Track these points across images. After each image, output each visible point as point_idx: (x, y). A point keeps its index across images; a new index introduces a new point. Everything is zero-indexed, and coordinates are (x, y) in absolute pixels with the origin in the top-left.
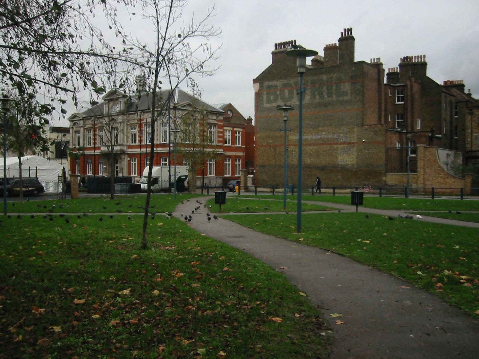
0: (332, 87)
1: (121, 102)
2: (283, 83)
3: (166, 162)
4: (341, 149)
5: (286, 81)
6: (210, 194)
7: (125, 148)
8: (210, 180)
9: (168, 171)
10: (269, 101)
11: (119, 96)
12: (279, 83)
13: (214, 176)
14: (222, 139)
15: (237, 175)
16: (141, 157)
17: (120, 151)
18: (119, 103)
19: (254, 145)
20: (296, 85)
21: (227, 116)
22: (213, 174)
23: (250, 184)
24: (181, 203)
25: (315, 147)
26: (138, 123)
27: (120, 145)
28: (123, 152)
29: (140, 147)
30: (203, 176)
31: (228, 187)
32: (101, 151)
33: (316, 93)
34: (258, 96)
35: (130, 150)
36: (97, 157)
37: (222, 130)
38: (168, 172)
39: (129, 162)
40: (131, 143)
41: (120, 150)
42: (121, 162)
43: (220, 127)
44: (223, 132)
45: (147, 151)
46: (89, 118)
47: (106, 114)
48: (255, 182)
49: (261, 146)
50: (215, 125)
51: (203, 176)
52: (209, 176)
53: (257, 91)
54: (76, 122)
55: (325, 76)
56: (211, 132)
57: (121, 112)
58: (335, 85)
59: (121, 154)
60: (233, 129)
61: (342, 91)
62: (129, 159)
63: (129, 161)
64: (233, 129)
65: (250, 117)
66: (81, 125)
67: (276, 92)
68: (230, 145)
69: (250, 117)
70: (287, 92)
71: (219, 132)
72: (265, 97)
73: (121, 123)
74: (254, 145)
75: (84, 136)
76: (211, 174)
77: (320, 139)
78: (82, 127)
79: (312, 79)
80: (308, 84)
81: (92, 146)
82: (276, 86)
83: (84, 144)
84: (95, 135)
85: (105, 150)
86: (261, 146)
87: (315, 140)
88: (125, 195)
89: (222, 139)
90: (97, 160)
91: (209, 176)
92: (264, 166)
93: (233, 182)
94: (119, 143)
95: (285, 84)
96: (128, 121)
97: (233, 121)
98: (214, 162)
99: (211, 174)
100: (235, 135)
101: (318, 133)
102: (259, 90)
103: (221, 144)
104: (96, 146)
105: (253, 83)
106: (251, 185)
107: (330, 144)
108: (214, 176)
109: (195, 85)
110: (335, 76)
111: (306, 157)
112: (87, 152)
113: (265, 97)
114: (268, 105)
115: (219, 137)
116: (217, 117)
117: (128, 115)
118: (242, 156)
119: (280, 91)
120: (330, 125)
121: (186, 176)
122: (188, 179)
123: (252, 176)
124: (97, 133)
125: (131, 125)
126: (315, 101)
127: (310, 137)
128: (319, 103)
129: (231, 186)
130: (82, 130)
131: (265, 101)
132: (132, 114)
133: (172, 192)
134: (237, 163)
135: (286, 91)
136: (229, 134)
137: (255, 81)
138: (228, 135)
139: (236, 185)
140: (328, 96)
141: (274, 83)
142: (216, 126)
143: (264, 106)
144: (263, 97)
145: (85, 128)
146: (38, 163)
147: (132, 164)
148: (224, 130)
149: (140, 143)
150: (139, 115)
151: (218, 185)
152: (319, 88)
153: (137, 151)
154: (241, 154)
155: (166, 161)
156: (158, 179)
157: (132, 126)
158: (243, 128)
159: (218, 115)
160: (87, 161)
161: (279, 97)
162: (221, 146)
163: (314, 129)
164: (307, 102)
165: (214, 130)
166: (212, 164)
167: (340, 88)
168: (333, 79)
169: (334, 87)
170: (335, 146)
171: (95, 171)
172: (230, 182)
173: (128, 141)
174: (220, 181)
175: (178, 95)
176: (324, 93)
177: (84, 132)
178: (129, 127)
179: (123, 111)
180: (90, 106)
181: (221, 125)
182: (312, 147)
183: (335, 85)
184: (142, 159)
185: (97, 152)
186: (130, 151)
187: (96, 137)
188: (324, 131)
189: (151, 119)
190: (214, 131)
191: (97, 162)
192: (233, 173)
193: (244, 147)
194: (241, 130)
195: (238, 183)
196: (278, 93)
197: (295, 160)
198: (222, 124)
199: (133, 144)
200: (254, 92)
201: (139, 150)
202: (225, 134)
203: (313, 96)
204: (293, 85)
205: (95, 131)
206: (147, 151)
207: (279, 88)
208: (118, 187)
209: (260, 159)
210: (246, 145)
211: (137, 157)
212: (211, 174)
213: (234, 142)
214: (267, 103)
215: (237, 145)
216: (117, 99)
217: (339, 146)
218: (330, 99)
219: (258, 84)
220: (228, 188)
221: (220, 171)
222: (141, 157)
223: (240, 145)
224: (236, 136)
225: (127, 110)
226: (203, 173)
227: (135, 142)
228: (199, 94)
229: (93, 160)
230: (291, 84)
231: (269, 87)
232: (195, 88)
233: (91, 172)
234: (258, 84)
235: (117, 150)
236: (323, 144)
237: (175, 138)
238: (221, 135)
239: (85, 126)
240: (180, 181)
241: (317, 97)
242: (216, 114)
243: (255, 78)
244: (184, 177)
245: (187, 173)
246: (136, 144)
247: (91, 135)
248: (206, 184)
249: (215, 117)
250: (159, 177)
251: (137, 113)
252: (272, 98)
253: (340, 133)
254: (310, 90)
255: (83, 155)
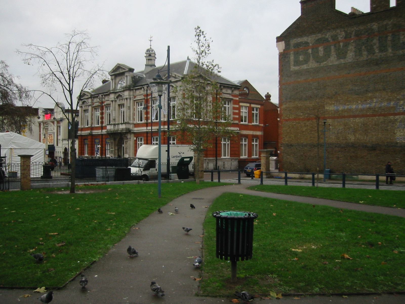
0: (387, 37)
1: (127, 76)
2: (317, 38)
3: (174, 142)
4: (401, 122)
5: (320, 36)
6: (222, 181)
7: (131, 127)
8: (224, 162)
9: (166, 151)
10: (297, 63)
11: (126, 70)
12: (310, 39)
13: (229, 157)
14: (237, 116)
15: (254, 157)
16: (147, 137)
17: (126, 130)
18: (126, 78)
19: (279, 119)
20: (333, 40)
21: (243, 92)
22: (228, 156)
23: (272, 168)
24: (157, 212)
25: (362, 120)
26: (144, 99)
27: (126, 123)
28: (129, 131)
29: (147, 125)
30: (216, 157)
31: (245, 171)
32: (107, 130)
33: (363, 47)
34: (283, 57)
35: (136, 129)
36: (104, 137)
37: (237, 106)
38: (167, 152)
39: (136, 141)
40: (137, 121)
41: (126, 128)
42: (126, 143)
43: (236, 102)
44: (239, 109)
45: (152, 129)
46: (97, 95)
47: (112, 91)
48: (280, 166)
49: (286, 120)
50: (230, 100)
51: (216, 157)
52: (223, 157)
53: (282, 51)
54: (85, 100)
55: (376, 24)
56: (225, 108)
57: (127, 87)
58: (390, 34)
59: (126, 133)
60: (250, 105)
61: (401, 42)
62: (135, 138)
63: (135, 140)
64: (250, 105)
65: (268, 93)
66: (89, 104)
67: (308, 50)
68: (247, 123)
69: (268, 93)
70: (322, 49)
71: (234, 108)
72: (292, 58)
73: (127, 99)
74: (279, 119)
75: (92, 115)
76: (225, 156)
77: (370, 108)
78: (90, 105)
79: (357, 29)
80: (351, 37)
81: (100, 125)
82: (307, 43)
83: (92, 124)
84: (102, 114)
85: (111, 129)
86: (286, 120)
87: (362, 110)
88: (103, 184)
89: (237, 116)
90: (104, 140)
91: (223, 157)
92: (291, 145)
93: (252, 165)
94: (125, 121)
95: (318, 39)
96: (135, 97)
97: (250, 97)
98: (228, 141)
99: (226, 156)
100: (253, 112)
101: (366, 101)
102: (284, 50)
103: (236, 122)
104: (104, 125)
105: (277, 41)
106: (274, 169)
107: (384, 115)
108: (229, 157)
109: (201, 34)
110: (390, 23)
111: (349, 134)
112: (95, 132)
113: (292, 58)
114: (297, 68)
115: (234, 114)
116: (233, 91)
117: (134, 90)
118: (260, 135)
119: (313, 49)
120: (384, 89)
121: (191, 158)
122: (193, 161)
123: (275, 158)
124: (104, 111)
125: (137, 101)
126: (361, 59)
127: (354, 107)
128: (367, 60)
129: (249, 170)
130: (90, 108)
131: (292, 63)
132: (138, 89)
133: (171, 179)
134: (254, 143)
135: (321, 49)
136: (246, 111)
137: (279, 39)
138: (244, 112)
139: (254, 168)
140: (381, 51)
141: (305, 39)
142: (230, 101)
143: (291, 70)
144: (290, 58)
145: (94, 107)
146: (13, 141)
147: (139, 144)
148: (240, 107)
149: (147, 121)
150: (146, 90)
151: (233, 168)
152: (367, 41)
153: (144, 129)
154: (259, 133)
155: (174, 140)
156: (155, 161)
157: (138, 102)
158: (261, 105)
159: (233, 89)
160: (95, 141)
161: (311, 57)
162: (237, 124)
163: (361, 96)
164: (350, 61)
165: (228, 106)
166: (225, 143)
167: (399, 38)
168: (388, 27)
169: (389, 38)
170: (392, 117)
171: (92, 152)
172: (247, 165)
173: (134, 119)
174: (235, 164)
175: (189, 67)
176: (375, 47)
177: (92, 111)
178: (136, 103)
179: (129, 86)
180: (101, 84)
181: (237, 100)
182: (357, 120)
183: (390, 34)
184: (148, 139)
185: (104, 131)
186: (136, 129)
187: (103, 116)
188: (376, 98)
189: (263, 177)
190: (229, 107)
191: (104, 143)
192: (250, 154)
193: (262, 126)
194: (259, 106)
195: (258, 167)
196: (310, 51)
197: (333, 137)
198: (237, 99)
199: (140, 122)
200: (278, 53)
201: (145, 128)
202: (241, 111)
203: (359, 52)
204: (329, 39)
205: (102, 109)
206: (152, 129)
207: (311, 45)
208: (99, 172)
209: (286, 136)
210: (265, 124)
211: (143, 136)
212: (226, 156)
213: (251, 120)
214: (294, 65)
215: (255, 123)
216: (123, 74)
217: (397, 117)
218: (383, 54)
219: (283, 42)
220: (245, 172)
221: (235, 152)
222: (147, 137)
223: (258, 124)
224: (254, 113)
225: (133, 85)
226: (217, 154)
227: (141, 120)
228: (207, 45)
229: (101, 140)
230: (327, 39)
231: (297, 45)
232: (202, 38)
233: (99, 153)
234: (283, 42)
235: (123, 129)
236: (375, 116)
237: (160, 94)
238: (237, 111)
239: (93, 105)
240: (183, 163)
241: (365, 53)
242: (231, 88)
243: (279, 35)
244: (188, 159)
245: (192, 154)
246: (143, 122)
247: (98, 113)
248: (218, 167)
249: (229, 91)
250: (156, 159)
251: (144, 88)
252: (301, 58)
253: (399, 100)
254: (354, 44)
255: (91, 135)
